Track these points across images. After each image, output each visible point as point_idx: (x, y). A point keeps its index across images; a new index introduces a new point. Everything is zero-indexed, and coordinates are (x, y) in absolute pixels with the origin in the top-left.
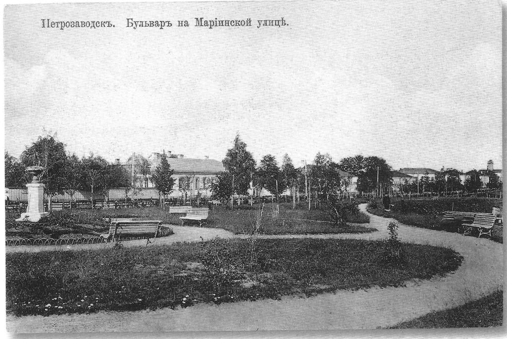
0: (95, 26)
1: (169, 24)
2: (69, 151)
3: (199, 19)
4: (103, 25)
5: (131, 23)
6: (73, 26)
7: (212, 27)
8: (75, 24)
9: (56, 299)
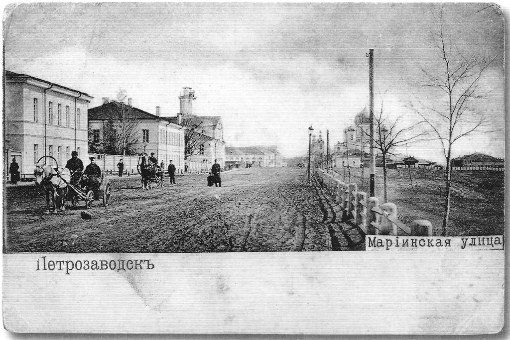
0: (125, 267)
1: (149, 265)
8: (90, 265)
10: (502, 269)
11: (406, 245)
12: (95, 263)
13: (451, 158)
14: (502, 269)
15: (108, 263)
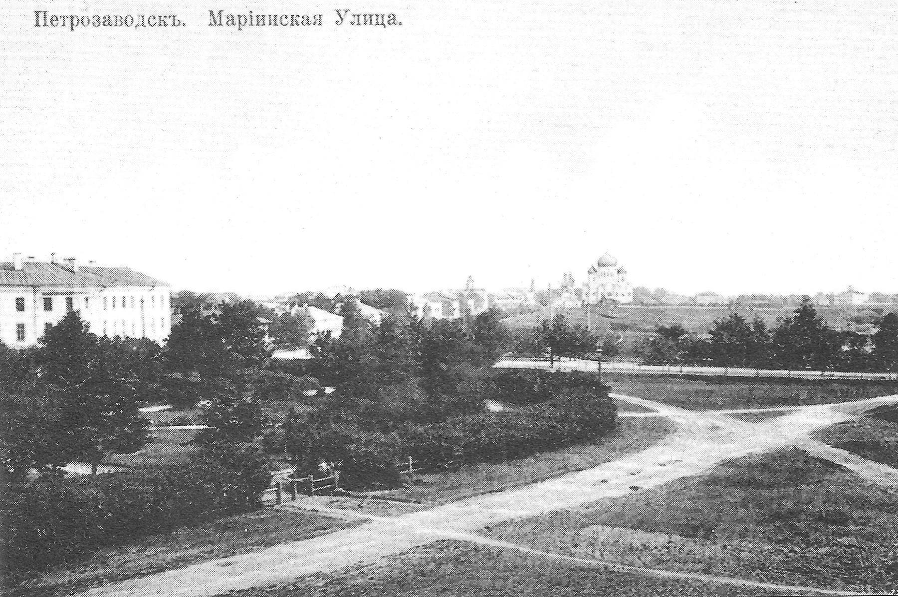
3: (216, 13)
5: (216, 19)
6: (97, 24)
8: (102, 20)
9: (178, 375)
12: (107, 18)
13: (53, 297)
15: (124, 18)
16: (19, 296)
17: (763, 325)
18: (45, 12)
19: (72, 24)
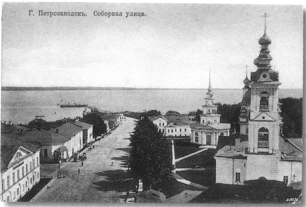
0: (74, 15)
1: (83, 14)
2: (272, 63)
4: (79, 15)
7: (110, 16)
8: (60, 14)
10: (302, 16)
11: (135, 15)
14: (302, 16)
16: (172, 129)
17: (109, 174)
18: (42, 11)
19: (51, 15)
